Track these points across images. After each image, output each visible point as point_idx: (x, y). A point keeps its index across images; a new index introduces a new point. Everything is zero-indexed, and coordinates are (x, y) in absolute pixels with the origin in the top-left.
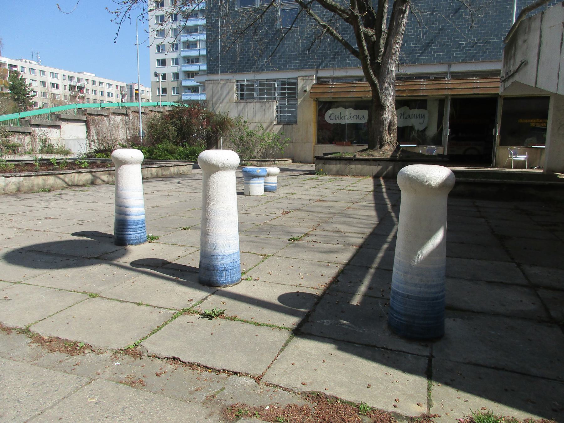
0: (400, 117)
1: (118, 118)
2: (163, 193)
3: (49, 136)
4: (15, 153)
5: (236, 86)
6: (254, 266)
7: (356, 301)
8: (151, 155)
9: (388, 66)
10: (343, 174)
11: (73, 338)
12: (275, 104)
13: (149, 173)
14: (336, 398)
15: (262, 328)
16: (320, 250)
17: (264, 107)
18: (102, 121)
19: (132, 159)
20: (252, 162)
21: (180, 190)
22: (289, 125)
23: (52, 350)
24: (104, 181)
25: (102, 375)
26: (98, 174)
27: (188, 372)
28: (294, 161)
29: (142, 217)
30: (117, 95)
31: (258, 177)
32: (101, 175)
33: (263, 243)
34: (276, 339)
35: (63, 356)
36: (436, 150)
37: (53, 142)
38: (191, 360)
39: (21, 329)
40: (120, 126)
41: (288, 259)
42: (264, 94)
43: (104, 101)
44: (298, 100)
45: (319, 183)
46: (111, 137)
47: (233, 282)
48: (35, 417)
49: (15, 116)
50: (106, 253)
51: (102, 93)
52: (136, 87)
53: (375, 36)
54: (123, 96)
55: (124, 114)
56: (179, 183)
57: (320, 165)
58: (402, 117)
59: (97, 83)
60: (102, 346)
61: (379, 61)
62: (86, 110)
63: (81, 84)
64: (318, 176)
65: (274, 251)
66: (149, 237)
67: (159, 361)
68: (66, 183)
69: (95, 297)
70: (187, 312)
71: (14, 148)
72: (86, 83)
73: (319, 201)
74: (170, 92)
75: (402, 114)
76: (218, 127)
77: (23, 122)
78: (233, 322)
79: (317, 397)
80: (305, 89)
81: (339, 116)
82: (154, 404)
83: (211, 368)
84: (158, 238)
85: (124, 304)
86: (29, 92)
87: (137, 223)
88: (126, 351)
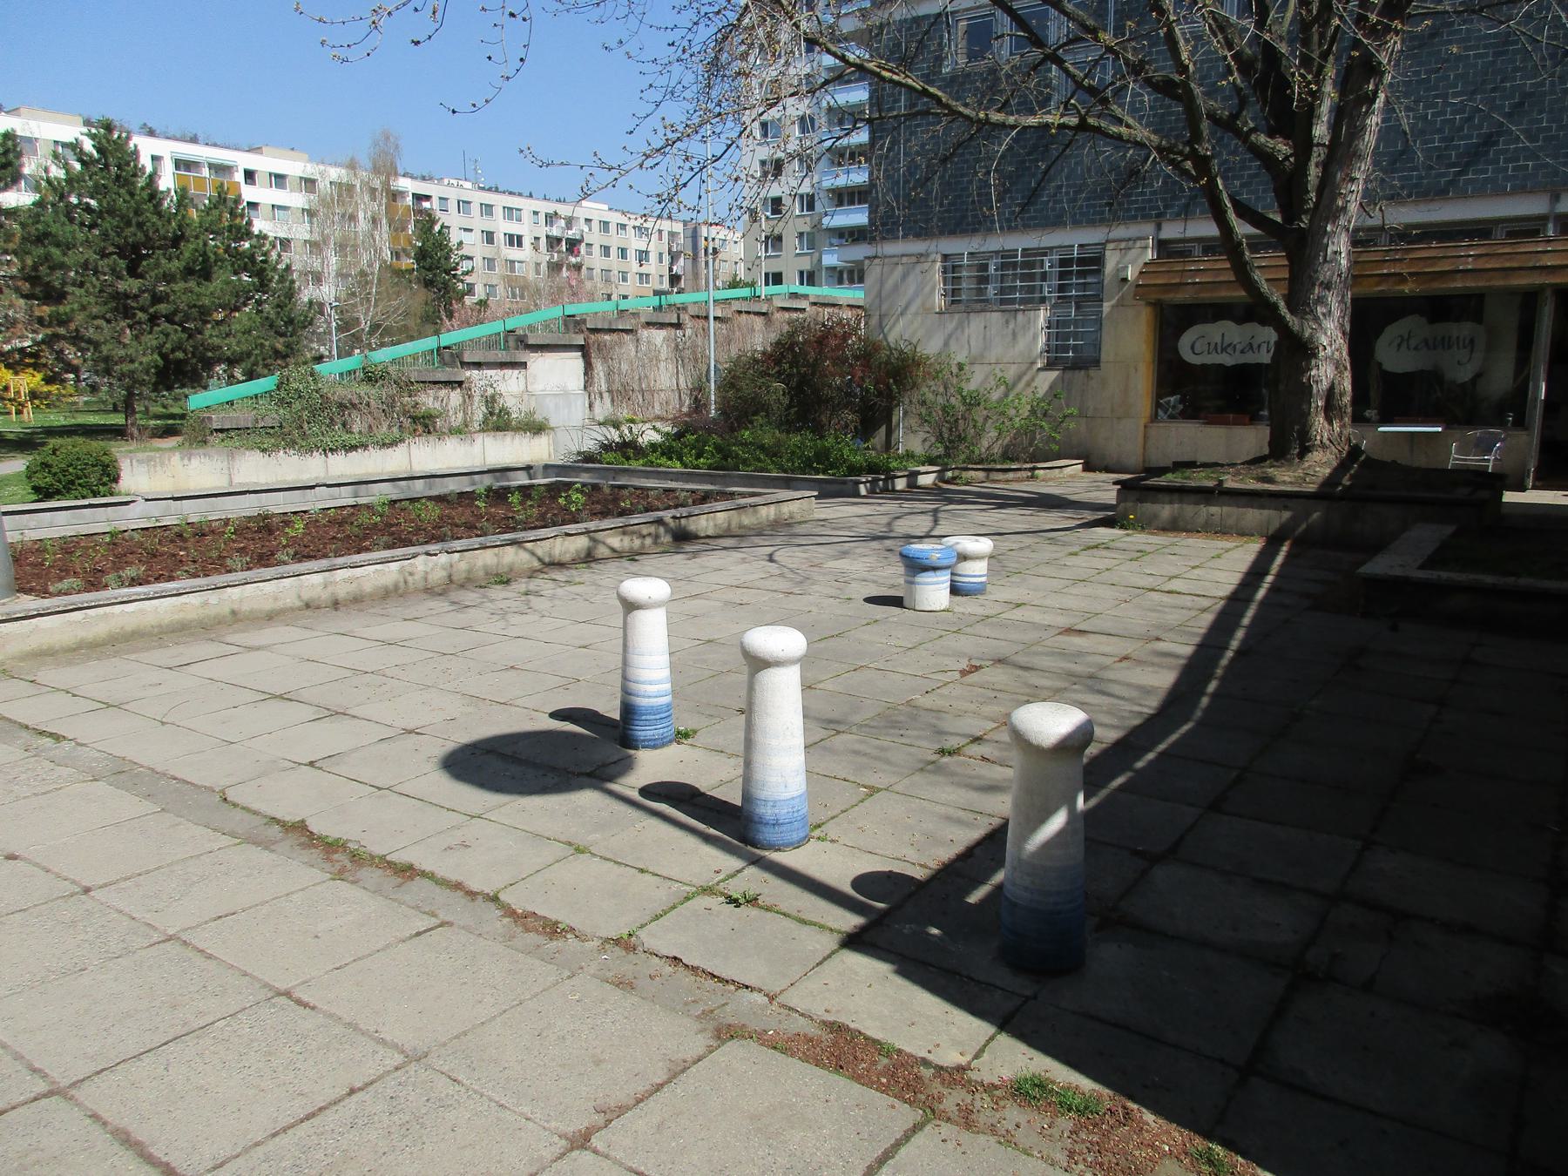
0: (1399, 345)
1: (659, 336)
2: (733, 595)
3: (501, 388)
4: (429, 432)
5: (941, 270)
6: (843, 812)
7: (974, 898)
8: (725, 458)
9: (1325, 241)
10: (1189, 527)
11: (553, 917)
12: (1042, 316)
13: (711, 524)
14: (860, 1032)
15: (807, 928)
16: (976, 782)
17: (1011, 326)
18: (621, 344)
19: (650, 601)
20: (972, 473)
21: (769, 584)
22: (1077, 372)
23: (527, 930)
24: (614, 550)
25: (585, 969)
26: (599, 536)
27: (688, 979)
28: (1088, 468)
29: (667, 699)
30: (661, 254)
31: (935, 569)
32: (608, 536)
33: (876, 758)
34: (818, 947)
35: (541, 939)
36: (1502, 441)
37: (510, 403)
38: (696, 964)
39: (488, 894)
40: (663, 356)
41: (910, 798)
42: (1013, 289)
43: (627, 273)
44: (1105, 304)
45: (1102, 564)
46: (640, 384)
47: (792, 844)
48: (513, 1007)
49: (429, 343)
50: (604, 765)
51: (623, 252)
52: (704, 231)
53: (1292, 159)
54: (674, 258)
55: (671, 325)
56: (771, 559)
57: (1130, 504)
58: (1404, 345)
59: (612, 228)
60: (588, 931)
61: (1302, 225)
62: (584, 321)
63: (573, 231)
64: (1122, 532)
65: (893, 779)
66: (679, 733)
67: (657, 960)
68: (540, 560)
69: (583, 852)
70: (707, 891)
71: (427, 421)
72: (586, 229)
73: (1069, 631)
74: (791, 242)
75: (1406, 337)
76: (891, 381)
77: (447, 358)
78: (769, 915)
79: (837, 1028)
80: (1122, 275)
81: (1219, 345)
82: (641, 1011)
83: (718, 977)
84: (695, 732)
85: (622, 868)
86: (458, 264)
87: (655, 710)
88: (617, 942)
